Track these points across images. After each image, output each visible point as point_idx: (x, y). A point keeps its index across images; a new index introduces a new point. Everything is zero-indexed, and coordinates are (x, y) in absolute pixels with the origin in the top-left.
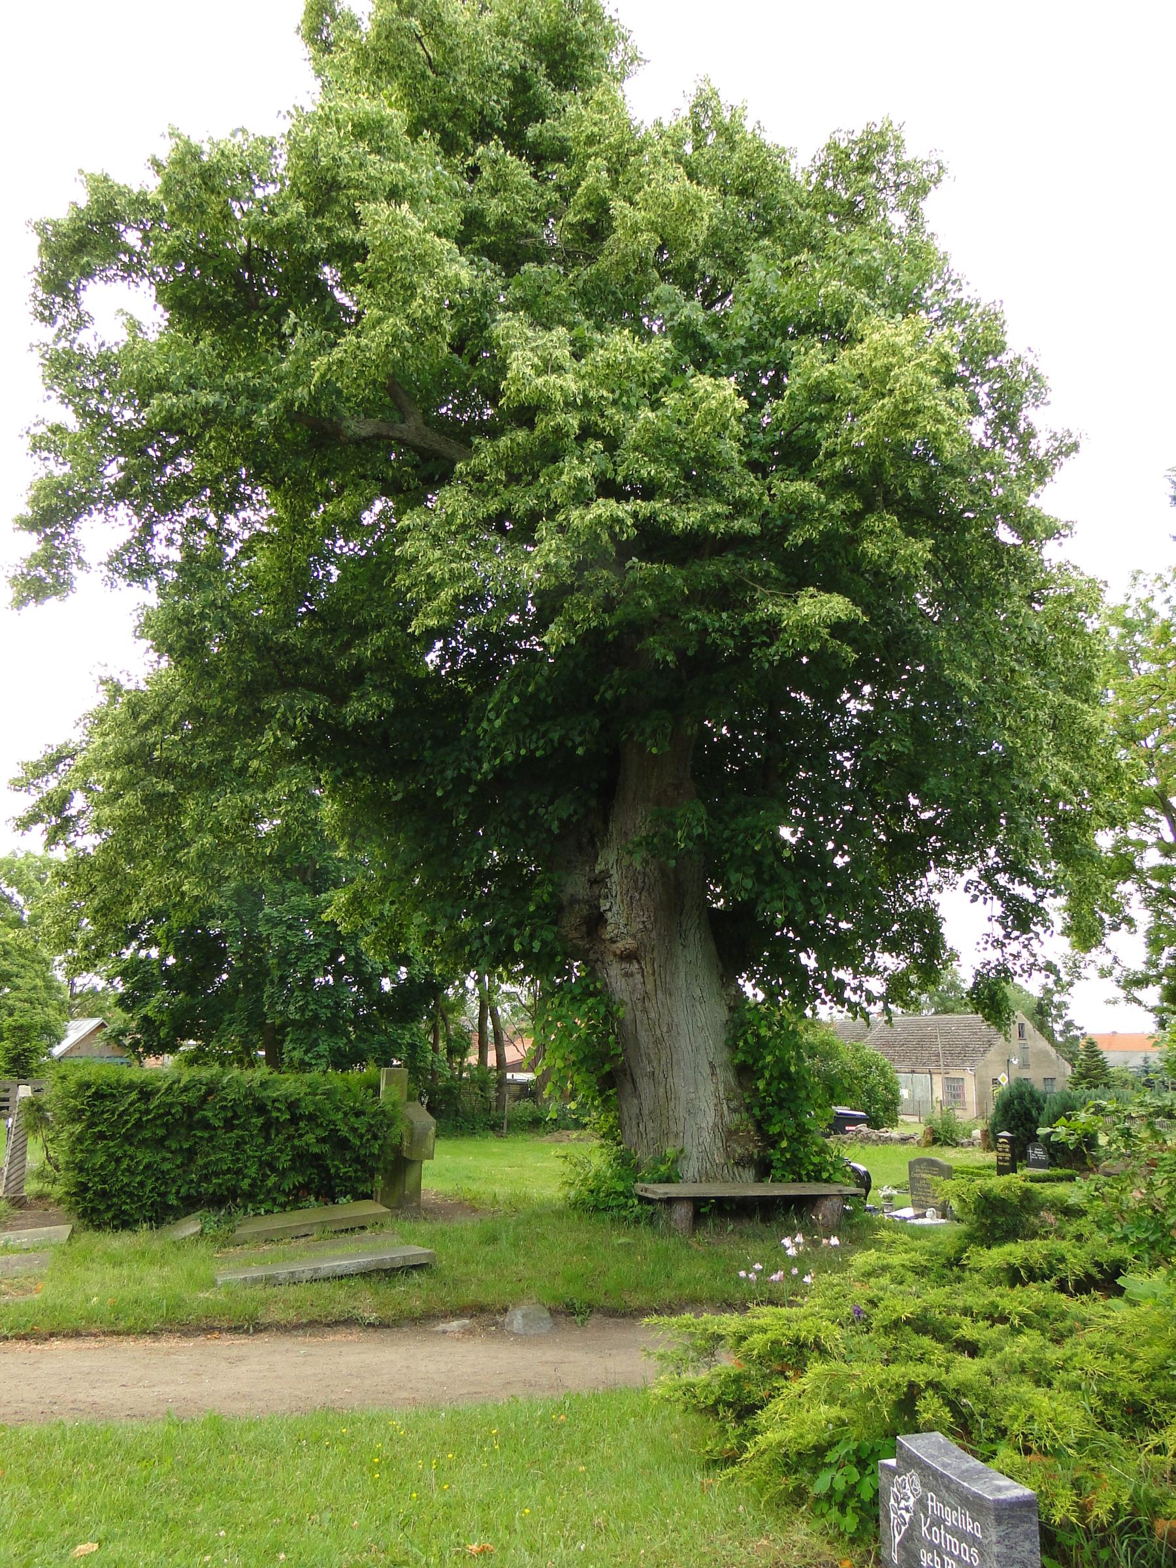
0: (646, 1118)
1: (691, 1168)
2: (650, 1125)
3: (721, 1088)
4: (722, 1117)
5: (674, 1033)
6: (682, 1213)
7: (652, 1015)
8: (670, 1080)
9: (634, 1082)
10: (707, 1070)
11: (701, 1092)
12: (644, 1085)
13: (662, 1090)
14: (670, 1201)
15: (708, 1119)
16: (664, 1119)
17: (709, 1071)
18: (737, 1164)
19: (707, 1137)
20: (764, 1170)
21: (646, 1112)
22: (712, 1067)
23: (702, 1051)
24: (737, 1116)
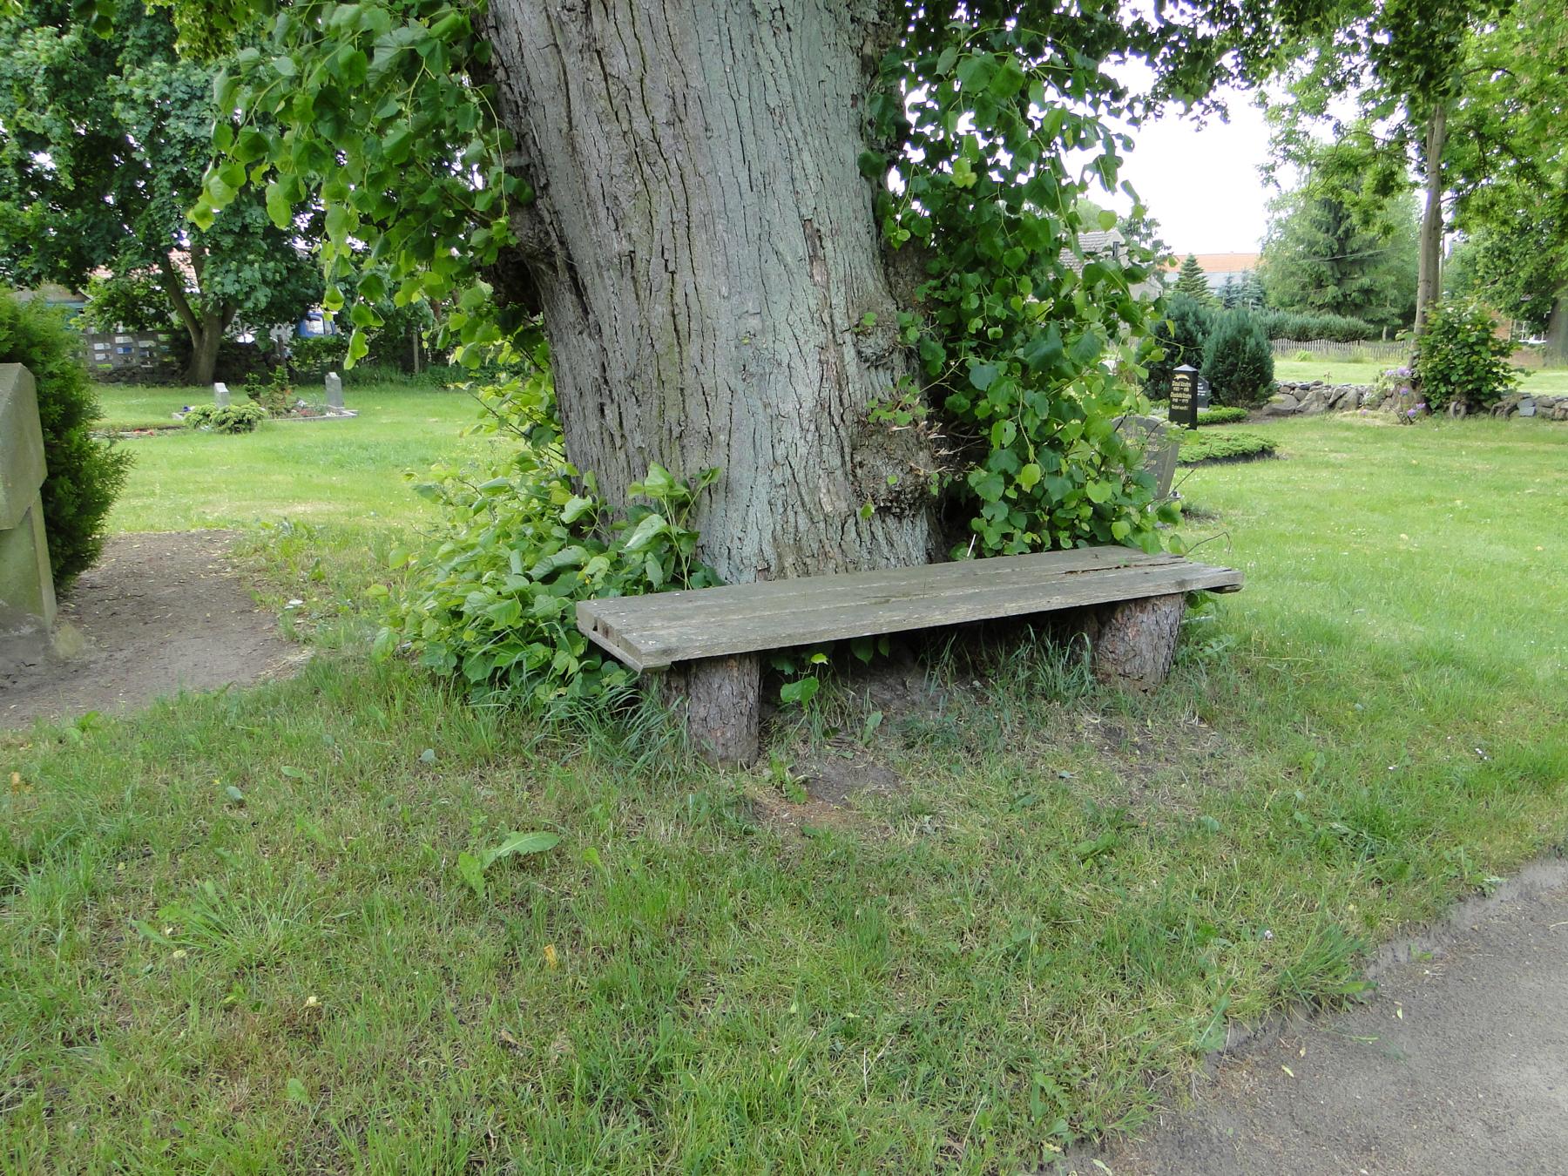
0: (620, 391)
1: (746, 528)
2: (631, 409)
3: (838, 300)
4: (841, 382)
5: (693, 125)
6: (733, 693)
7: (618, 65)
8: (684, 277)
9: (579, 289)
10: (794, 244)
11: (779, 310)
12: (606, 293)
13: (660, 310)
14: (684, 672)
15: (801, 390)
16: (672, 396)
17: (802, 249)
18: (883, 511)
19: (796, 442)
20: (952, 521)
21: (616, 374)
22: (814, 237)
23: (781, 186)
24: (882, 378)
